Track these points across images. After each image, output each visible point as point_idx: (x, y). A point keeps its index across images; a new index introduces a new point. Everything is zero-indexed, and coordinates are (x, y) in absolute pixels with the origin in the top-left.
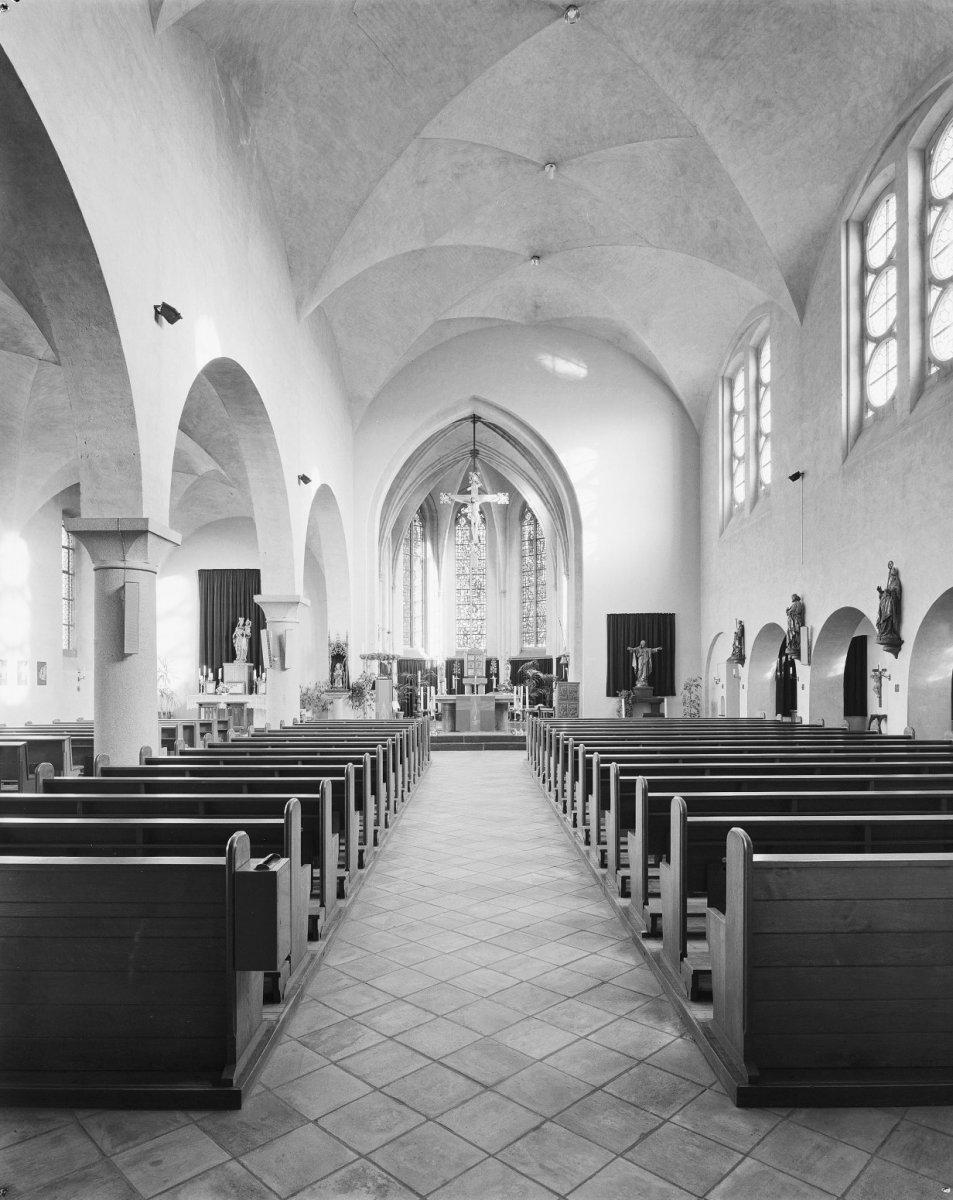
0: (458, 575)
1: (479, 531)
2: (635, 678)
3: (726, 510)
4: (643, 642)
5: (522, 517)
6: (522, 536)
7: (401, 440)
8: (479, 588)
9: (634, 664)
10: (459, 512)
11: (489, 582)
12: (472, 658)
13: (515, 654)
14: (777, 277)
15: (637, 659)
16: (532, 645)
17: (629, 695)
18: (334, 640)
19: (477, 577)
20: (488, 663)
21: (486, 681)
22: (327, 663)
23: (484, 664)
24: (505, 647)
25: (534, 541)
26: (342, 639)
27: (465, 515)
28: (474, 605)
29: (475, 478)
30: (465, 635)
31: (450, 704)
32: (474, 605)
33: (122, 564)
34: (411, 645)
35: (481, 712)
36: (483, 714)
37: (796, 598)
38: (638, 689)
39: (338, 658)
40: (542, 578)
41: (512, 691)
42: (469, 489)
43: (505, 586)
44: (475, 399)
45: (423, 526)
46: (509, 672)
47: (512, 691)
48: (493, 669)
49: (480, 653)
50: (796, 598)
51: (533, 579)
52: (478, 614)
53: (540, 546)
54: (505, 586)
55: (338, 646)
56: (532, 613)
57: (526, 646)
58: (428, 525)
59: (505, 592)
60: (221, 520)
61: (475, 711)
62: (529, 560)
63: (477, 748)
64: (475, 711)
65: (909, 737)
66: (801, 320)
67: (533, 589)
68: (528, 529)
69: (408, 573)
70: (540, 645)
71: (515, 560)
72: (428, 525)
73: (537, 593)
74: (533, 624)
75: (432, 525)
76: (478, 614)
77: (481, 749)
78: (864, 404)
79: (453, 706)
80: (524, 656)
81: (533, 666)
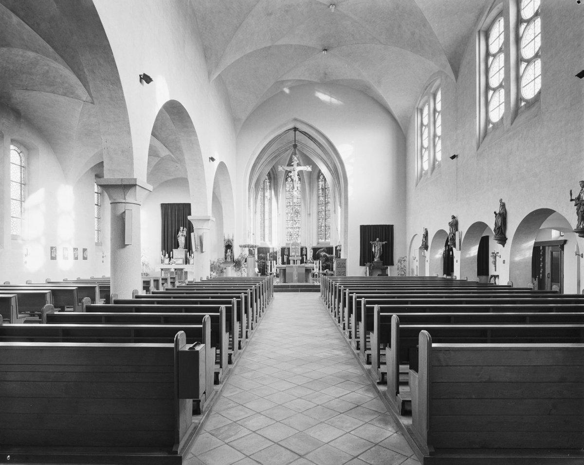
2: (374, 257)
3: (419, 176)
6: (318, 187)
9: (373, 250)
10: (288, 175)
13: (315, 245)
14: (444, 59)
15: (375, 247)
16: (323, 241)
17: (371, 265)
18: (226, 238)
19: (296, 207)
20: (302, 249)
21: (300, 258)
22: (223, 249)
24: (310, 241)
25: (324, 189)
26: (231, 238)
27: (291, 177)
29: (296, 158)
30: (291, 235)
32: (295, 221)
33: (124, 201)
36: (299, 275)
37: (454, 217)
39: (229, 247)
41: (313, 263)
42: (292, 164)
44: (295, 120)
45: (270, 182)
46: (312, 254)
47: (313, 263)
48: (304, 252)
49: (298, 244)
50: (454, 217)
51: (323, 208)
52: (297, 225)
55: (229, 241)
56: (323, 225)
57: (320, 241)
58: (272, 182)
59: (310, 214)
60: (173, 179)
62: (322, 199)
64: (295, 273)
65: (510, 286)
66: (457, 77)
67: (324, 213)
70: (327, 240)
71: (315, 198)
78: (488, 121)
79: (284, 270)
80: (319, 246)
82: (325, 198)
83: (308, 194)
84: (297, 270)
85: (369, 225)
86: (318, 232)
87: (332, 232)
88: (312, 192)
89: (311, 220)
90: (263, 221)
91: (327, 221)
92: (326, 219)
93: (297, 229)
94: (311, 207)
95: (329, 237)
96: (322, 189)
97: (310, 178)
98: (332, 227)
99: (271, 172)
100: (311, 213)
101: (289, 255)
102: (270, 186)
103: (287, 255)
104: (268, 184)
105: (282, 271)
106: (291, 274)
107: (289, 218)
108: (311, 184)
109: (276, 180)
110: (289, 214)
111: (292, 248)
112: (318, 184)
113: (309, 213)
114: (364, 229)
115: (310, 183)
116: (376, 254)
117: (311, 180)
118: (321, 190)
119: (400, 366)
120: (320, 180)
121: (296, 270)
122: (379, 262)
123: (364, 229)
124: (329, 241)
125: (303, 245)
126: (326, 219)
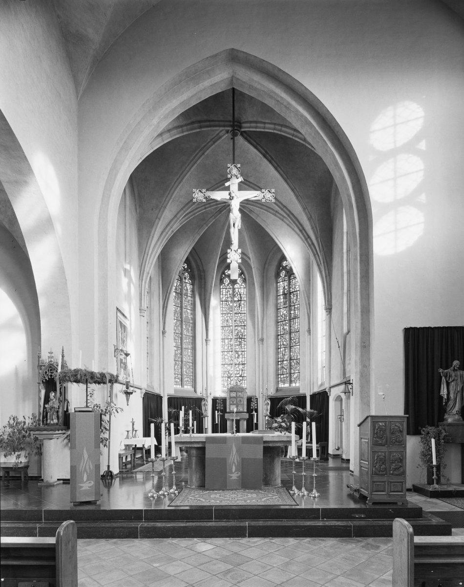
0: (222, 314)
1: (241, 288)
2: (443, 410)
4: (456, 363)
5: (278, 275)
6: (277, 291)
7: (143, 121)
8: (241, 338)
9: (444, 392)
10: (224, 273)
11: (249, 332)
12: (233, 394)
13: (272, 392)
15: (448, 384)
16: (287, 385)
17: (439, 433)
19: (239, 328)
20: (249, 400)
21: (247, 416)
23: (245, 403)
24: (261, 385)
25: (287, 295)
27: (229, 276)
28: (237, 352)
29: (235, 171)
30: (229, 377)
31: (198, 448)
32: (237, 352)
34: (182, 385)
35: (243, 460)
36: (244, 464)
38: (450, 425)
40: (296, 326)
41: (288, 429)
42: (227, 184)
43: (262, 334)
44: (235, 57)
45: (193, 284)
46: (269, 407)
47: (288, 429)
48: (253, 405)
49: (243, 390)
51: (287, 327)
52: (240, 360)
53: (293, 298)
54: (262, 334)
56: (286, 357)
57: (281, 385)
58: (197, 282)
59: (262, 340)
61: (234, 458)
62: (283, 311)
63: (236, 533)
64: (234, 458)
67: (287, 337)
68: (282, 285)
69: (179, 323)
70: (293, 385)
71: (271, 311)
72: (197, 282)
73: (291, 339)
74: (287, 366)
75: (200, 283)
76: (240, 360)
77: (243, 535)
79: (202, 450)
80: (280, 394)
81: (292, 402)
82: (290, 310)
83: (259, 305)
84: (239, 451)
85: (429, 328)
86: (277, 370)
87: (304, 369)
88: (267, 301)
89: (265, 350)
90: (179, 351)
91: (293, 349)
92: (290, 347)
93: (241, 367)
94: (265, 327)
95: (298, 378)
96: (284, 294)
97: (263, 277)
98: (304, 360)
99: (191, 258)
100: (265, 337)
101: (224, 411)
102: (193, 291)
103: (222, 411)
104: (189, 287)
105: (194, 452)
106: (223, 463)
107: (226, 348)
108: (265, 289)
109: (203, 280)
110: (226, 341)
111: (231, 398)
112: (277, 287)
113: (260, 337)
114: (415, 339)
115: (263, 286)
116: (451, 403)
117: (265, 280)
118: (282, 297)
119: (227, 411)
120: (280, 280)
121: (234, 449)
122: (457, 425)
123: (415, 339)
124: (297, 385)
125: (249, 393)
126: (290, 347)
